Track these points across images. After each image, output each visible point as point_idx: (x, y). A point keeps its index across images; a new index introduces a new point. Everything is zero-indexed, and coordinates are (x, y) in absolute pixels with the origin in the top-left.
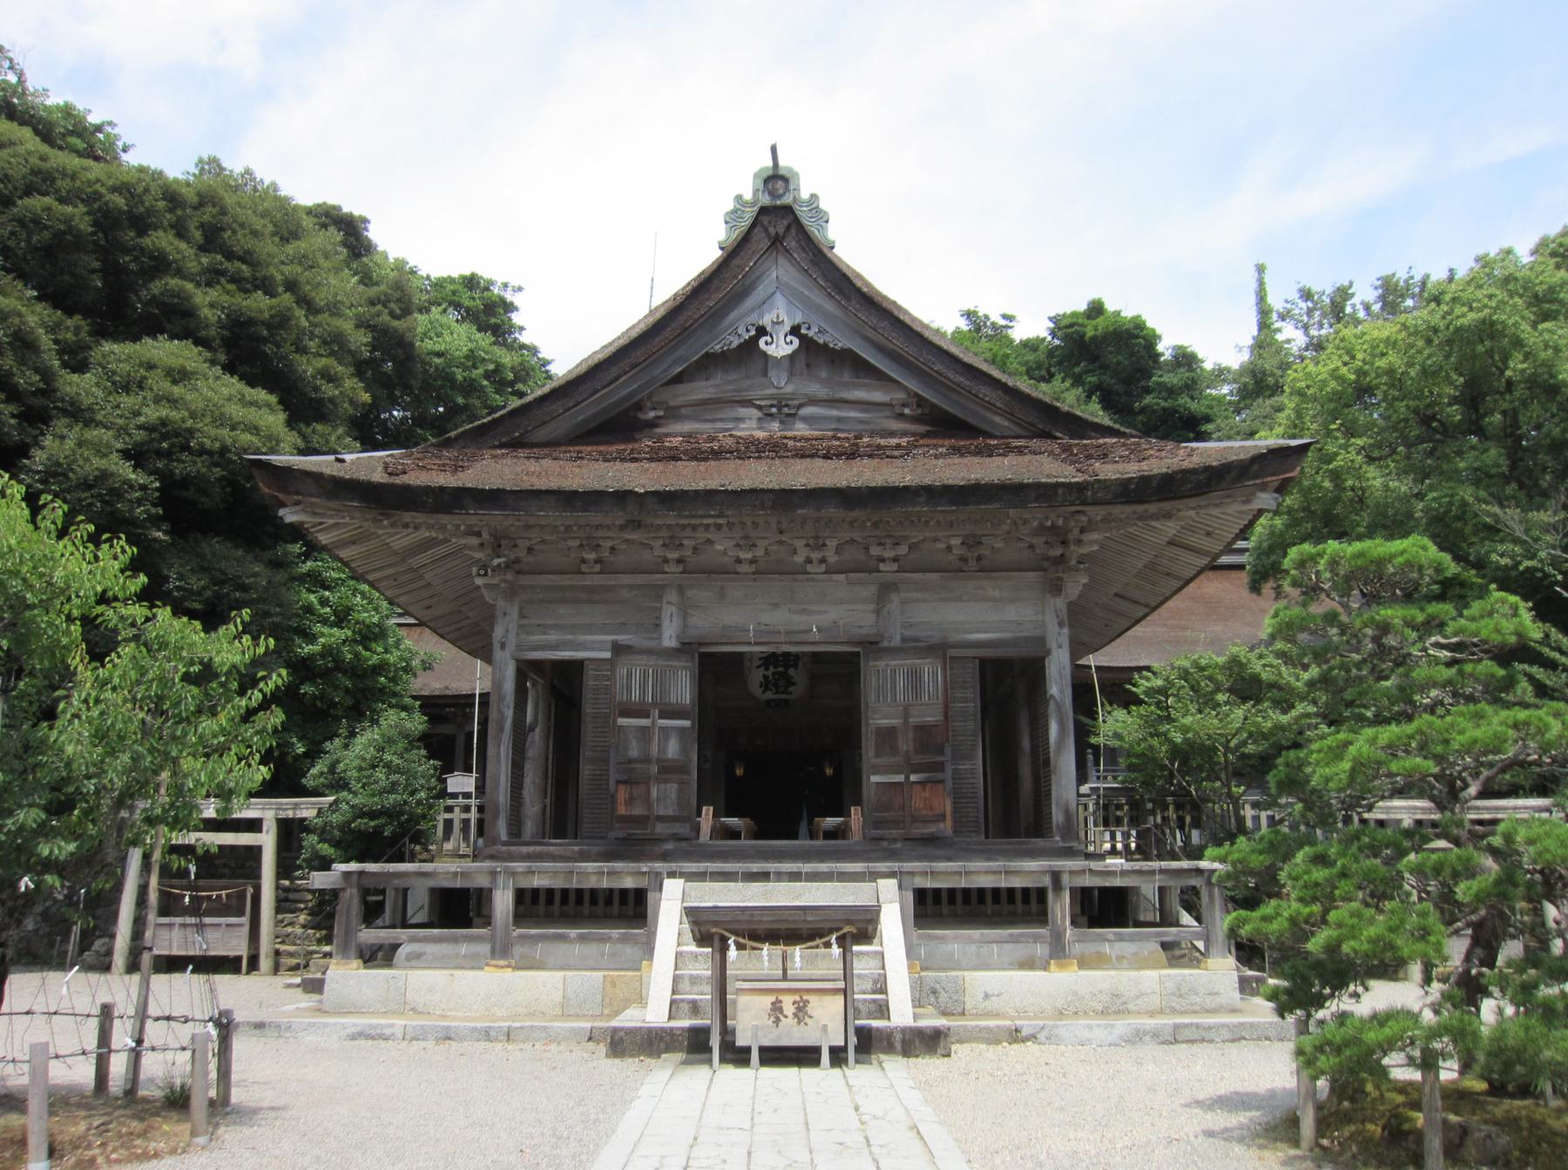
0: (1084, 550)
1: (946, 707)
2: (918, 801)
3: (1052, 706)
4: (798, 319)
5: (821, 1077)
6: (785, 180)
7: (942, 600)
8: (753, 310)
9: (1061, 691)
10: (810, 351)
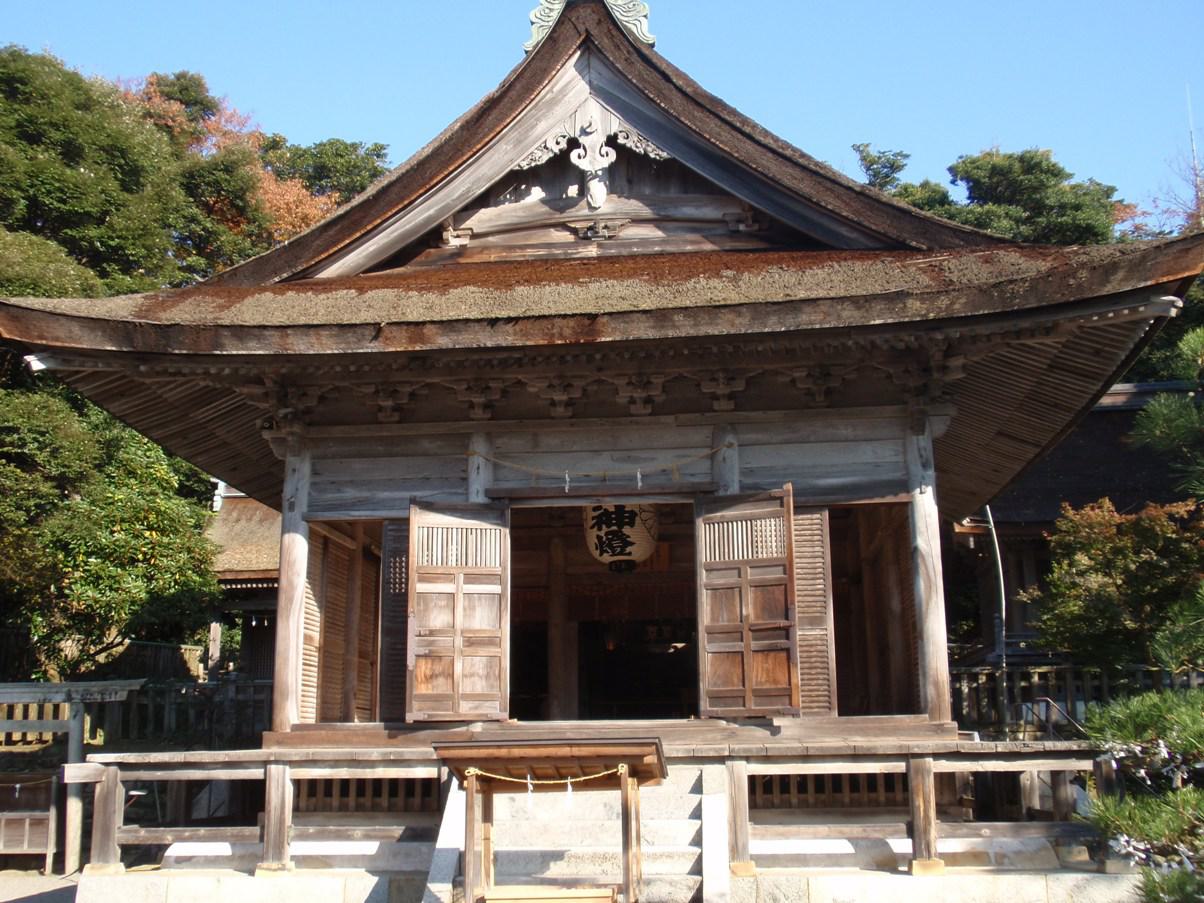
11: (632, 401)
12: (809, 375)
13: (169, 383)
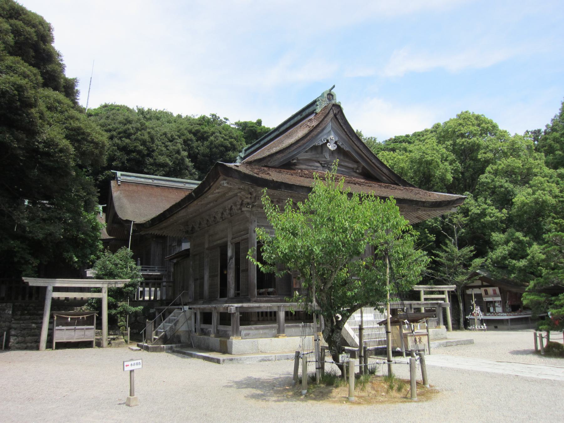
4: (337, 139)
6: (332, 96)
10: (339, 150)
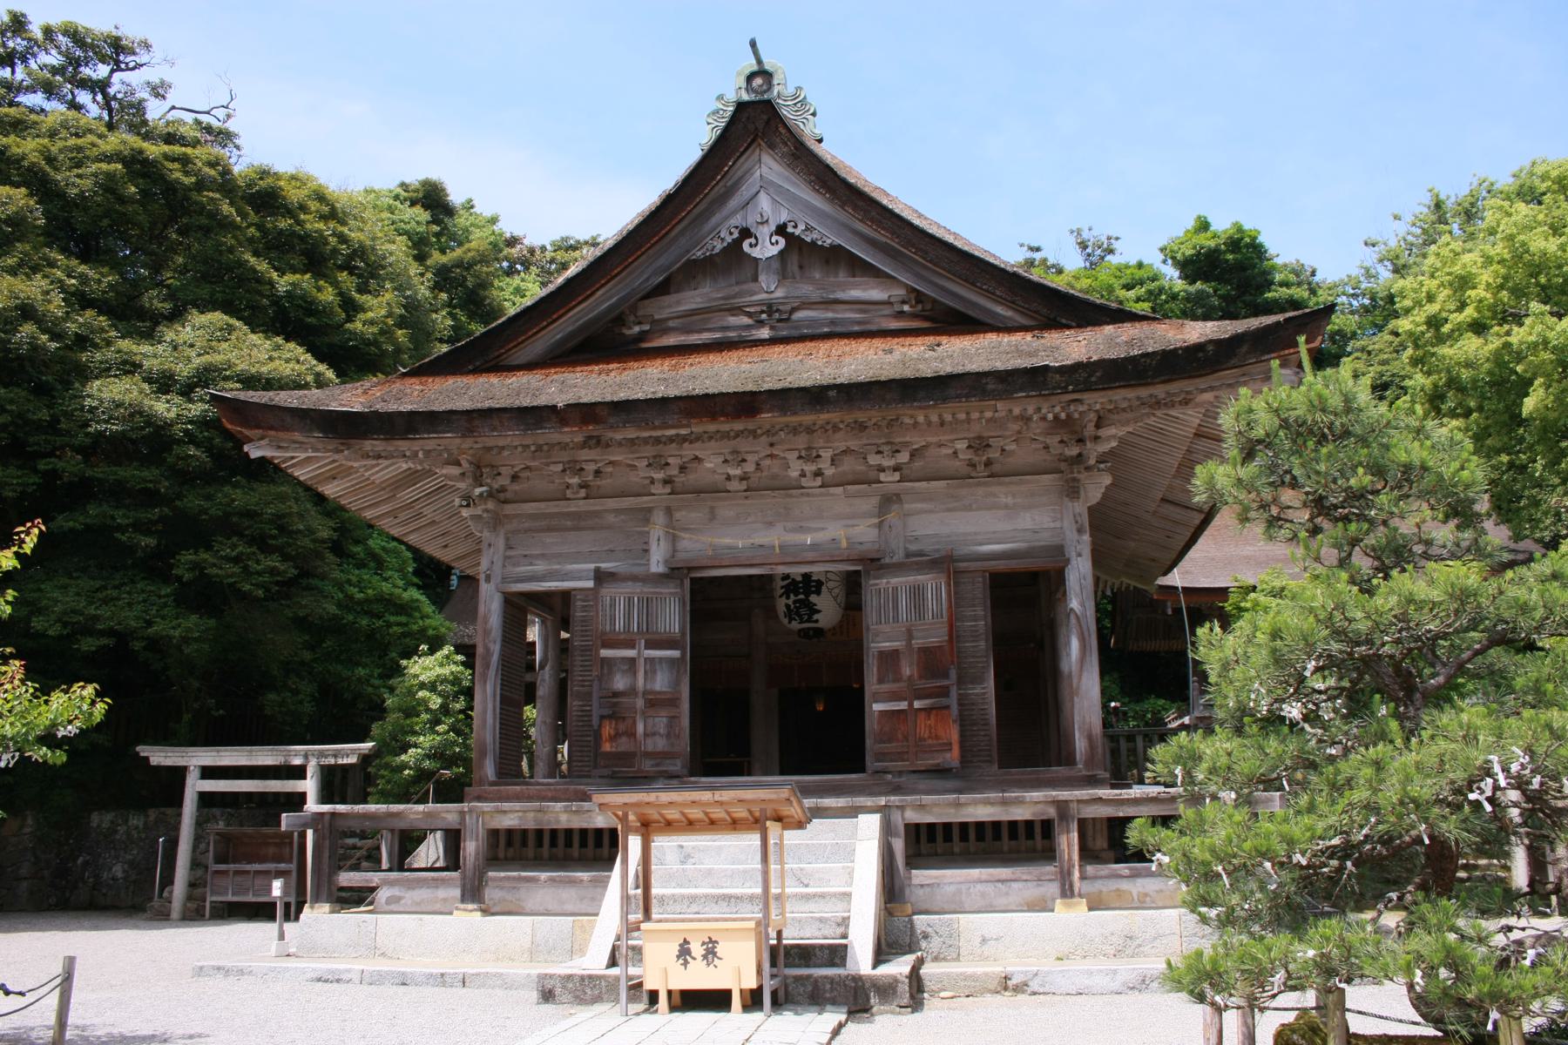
0: (1104, 447)
1: (951, 626)
2: (923, 727)
3: (1073, 620)
4: (784, 218)
5: (736, 1020)
7: (949, 510)
8: (734, 212)
9: (1082, 605)
10: (797, 250)
11: (803, 475)
12: (969, 447)
13: (374, 466)
